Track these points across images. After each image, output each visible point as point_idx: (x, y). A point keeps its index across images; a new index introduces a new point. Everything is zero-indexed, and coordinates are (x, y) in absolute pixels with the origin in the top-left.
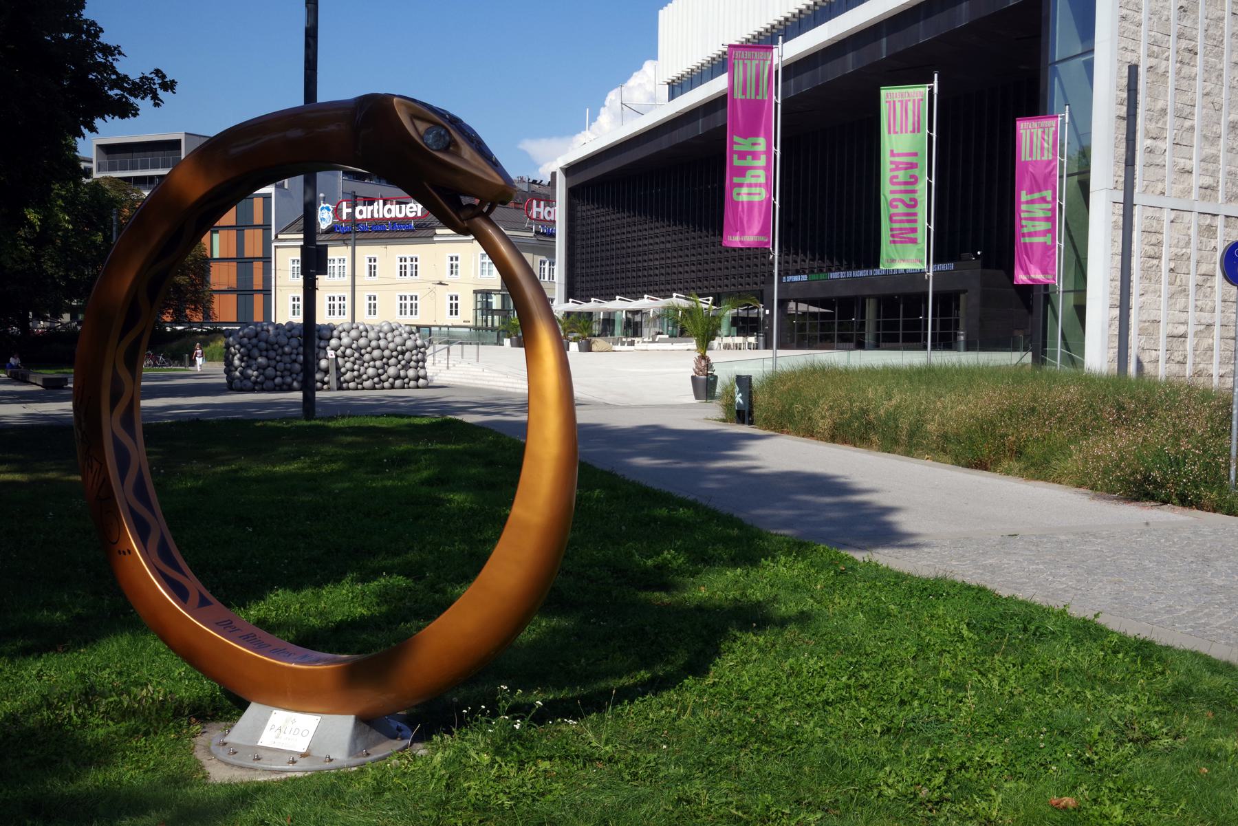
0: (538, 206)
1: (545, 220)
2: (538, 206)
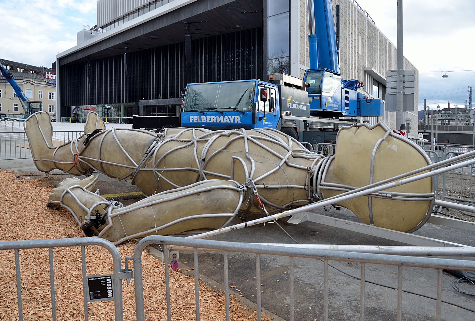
0: (48, 74)
1: (50, 79)
2: (48, 74)
